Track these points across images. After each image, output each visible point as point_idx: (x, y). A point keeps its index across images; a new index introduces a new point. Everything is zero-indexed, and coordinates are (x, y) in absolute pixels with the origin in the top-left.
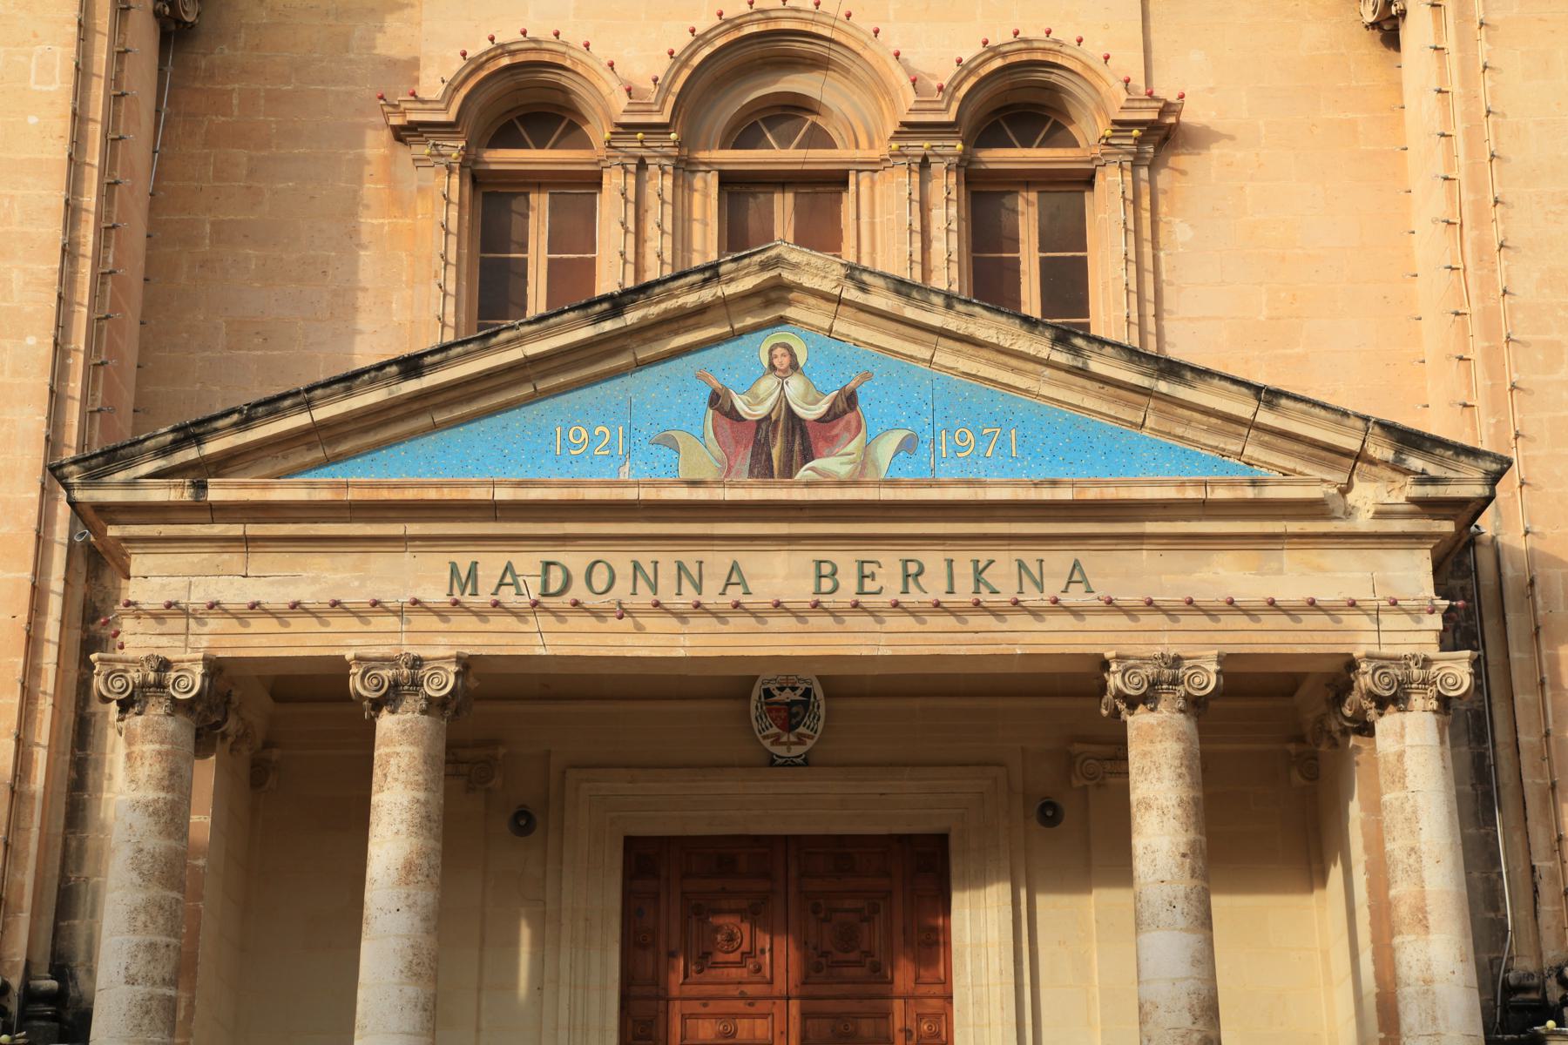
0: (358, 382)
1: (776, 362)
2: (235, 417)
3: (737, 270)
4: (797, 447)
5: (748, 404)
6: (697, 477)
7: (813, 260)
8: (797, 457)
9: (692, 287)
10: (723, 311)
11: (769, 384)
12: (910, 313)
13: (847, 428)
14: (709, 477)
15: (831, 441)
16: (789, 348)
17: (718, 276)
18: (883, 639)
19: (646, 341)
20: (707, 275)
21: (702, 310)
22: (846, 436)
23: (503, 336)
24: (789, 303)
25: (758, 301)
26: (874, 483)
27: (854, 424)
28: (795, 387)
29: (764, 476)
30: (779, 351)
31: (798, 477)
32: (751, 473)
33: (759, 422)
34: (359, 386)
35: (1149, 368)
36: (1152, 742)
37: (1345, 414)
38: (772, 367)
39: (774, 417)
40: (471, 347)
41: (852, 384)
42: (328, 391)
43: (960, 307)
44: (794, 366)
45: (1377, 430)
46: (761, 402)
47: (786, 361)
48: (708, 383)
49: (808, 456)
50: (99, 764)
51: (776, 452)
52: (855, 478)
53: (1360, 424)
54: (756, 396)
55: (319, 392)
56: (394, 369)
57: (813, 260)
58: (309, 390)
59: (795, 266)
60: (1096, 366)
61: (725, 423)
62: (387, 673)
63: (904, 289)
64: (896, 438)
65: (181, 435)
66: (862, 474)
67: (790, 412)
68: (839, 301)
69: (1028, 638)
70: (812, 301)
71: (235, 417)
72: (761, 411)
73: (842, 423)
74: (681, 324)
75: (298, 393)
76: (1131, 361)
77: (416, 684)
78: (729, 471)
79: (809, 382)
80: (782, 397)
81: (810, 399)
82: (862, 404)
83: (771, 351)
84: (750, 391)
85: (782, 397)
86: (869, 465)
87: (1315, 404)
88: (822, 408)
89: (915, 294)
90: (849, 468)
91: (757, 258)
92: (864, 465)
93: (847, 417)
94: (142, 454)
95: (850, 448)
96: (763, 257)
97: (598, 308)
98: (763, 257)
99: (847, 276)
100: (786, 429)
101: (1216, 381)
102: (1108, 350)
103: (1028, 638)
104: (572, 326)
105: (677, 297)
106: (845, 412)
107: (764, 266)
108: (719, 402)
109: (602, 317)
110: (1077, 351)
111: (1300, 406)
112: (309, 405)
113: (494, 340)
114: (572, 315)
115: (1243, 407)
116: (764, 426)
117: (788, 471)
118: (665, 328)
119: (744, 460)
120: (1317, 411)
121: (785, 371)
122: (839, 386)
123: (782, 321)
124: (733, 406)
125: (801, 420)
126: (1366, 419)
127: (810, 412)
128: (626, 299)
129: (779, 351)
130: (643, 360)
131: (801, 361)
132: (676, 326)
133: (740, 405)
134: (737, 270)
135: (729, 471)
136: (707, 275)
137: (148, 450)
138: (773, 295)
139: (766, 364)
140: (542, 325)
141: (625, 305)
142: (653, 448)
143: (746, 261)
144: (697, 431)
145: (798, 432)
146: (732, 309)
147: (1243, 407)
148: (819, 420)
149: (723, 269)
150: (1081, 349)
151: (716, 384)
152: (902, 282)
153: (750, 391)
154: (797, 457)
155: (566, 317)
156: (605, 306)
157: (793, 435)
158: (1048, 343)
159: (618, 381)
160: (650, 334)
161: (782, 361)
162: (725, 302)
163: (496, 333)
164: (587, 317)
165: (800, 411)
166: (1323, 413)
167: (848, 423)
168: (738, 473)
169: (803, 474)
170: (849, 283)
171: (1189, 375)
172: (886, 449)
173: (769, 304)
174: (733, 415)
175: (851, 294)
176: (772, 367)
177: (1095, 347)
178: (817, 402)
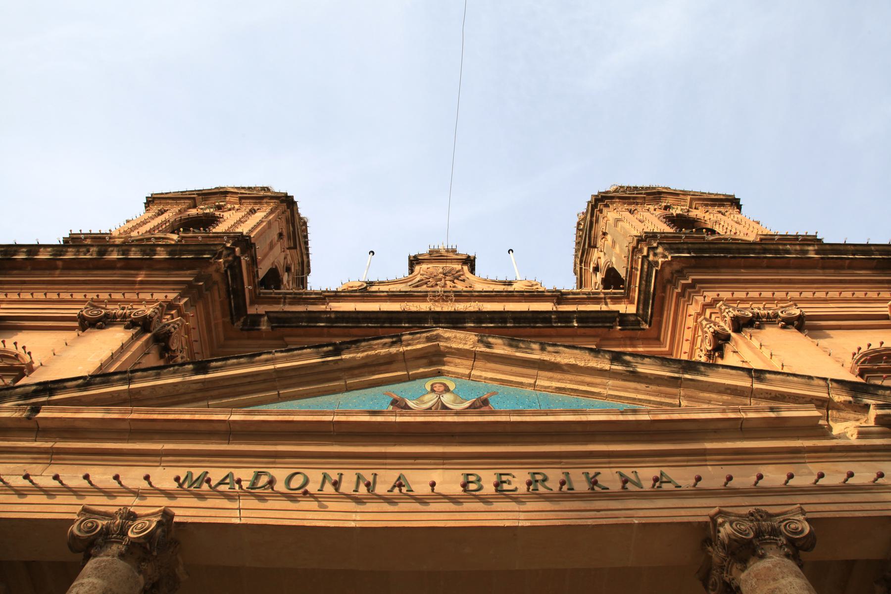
0: (165, 371)
2: (80, 381)
3: (412, 339)
6: (376, 409)
7: (458, 335)
9: (384, 345)
17: (401, 341)
18: (522, 516)
20: (394, 339)
23: (264, 357)
24: (444, 364)
25: (425, 361)
34: (165, 374)
35: (675, 366)
36: (774, 580)
37: (810, 378)
40: (242, 360)
42: (145, 374)
43: (550, 349)
45: (835, 385)
47: (442, 388)
53: (822, 383)
55: (139, 374)
56: (191, 366)
57: (458, 335)
58: (133, 371)
59: (448, 339)
60: (641, 369)
62: (102, 523)
65: (41, 387)
69: (641, 513)
71: (80, 381)
74: (377, 368)
75: (125, 372)
76: (664, 365)
77: (123, 532)
83: (432, 385)
84: (419, 399)
87: (788, 374)
91: (425, 335)
94: (11, 396)
96: (428, 334)
97: (325, 349)
98: (428, 334)
99: (479, 341)
101: (720, 369)
102: (647, 360)
103: (641, 513)
104: (309, 356)
105: (375, 349)
107: (429, 339)
109: (327, 354)
110: (627, 364)
111: (779, 377)
112: (130, 381)
113: (257, 358)
114: (309, 350)
115: (744, 382)
118: (366, 369)
120: (791, 378)
123: (440, 373)
124: (406, 404)
126: (825, 379)
128: (344, 346)
132: (373, 369)
134: (412, 339)
136: (394, 339)
137: (16, 394)
138: (434, 359)
140: (289, 354)
141: (343, 350)
143: (418, 335)
147: (744, 382)
149: (404, 338)
150: (629, 362)
155: (305, 351)
156: (330, 348)
158: (607, 361)
159: (333, 396)
160: (356, 372)
163: (260, 354)
164: (318, 353)
166: (795, 379)
170: (480, 345)
171: (702, 368)
173: (431, 364)
177: (639, 360)
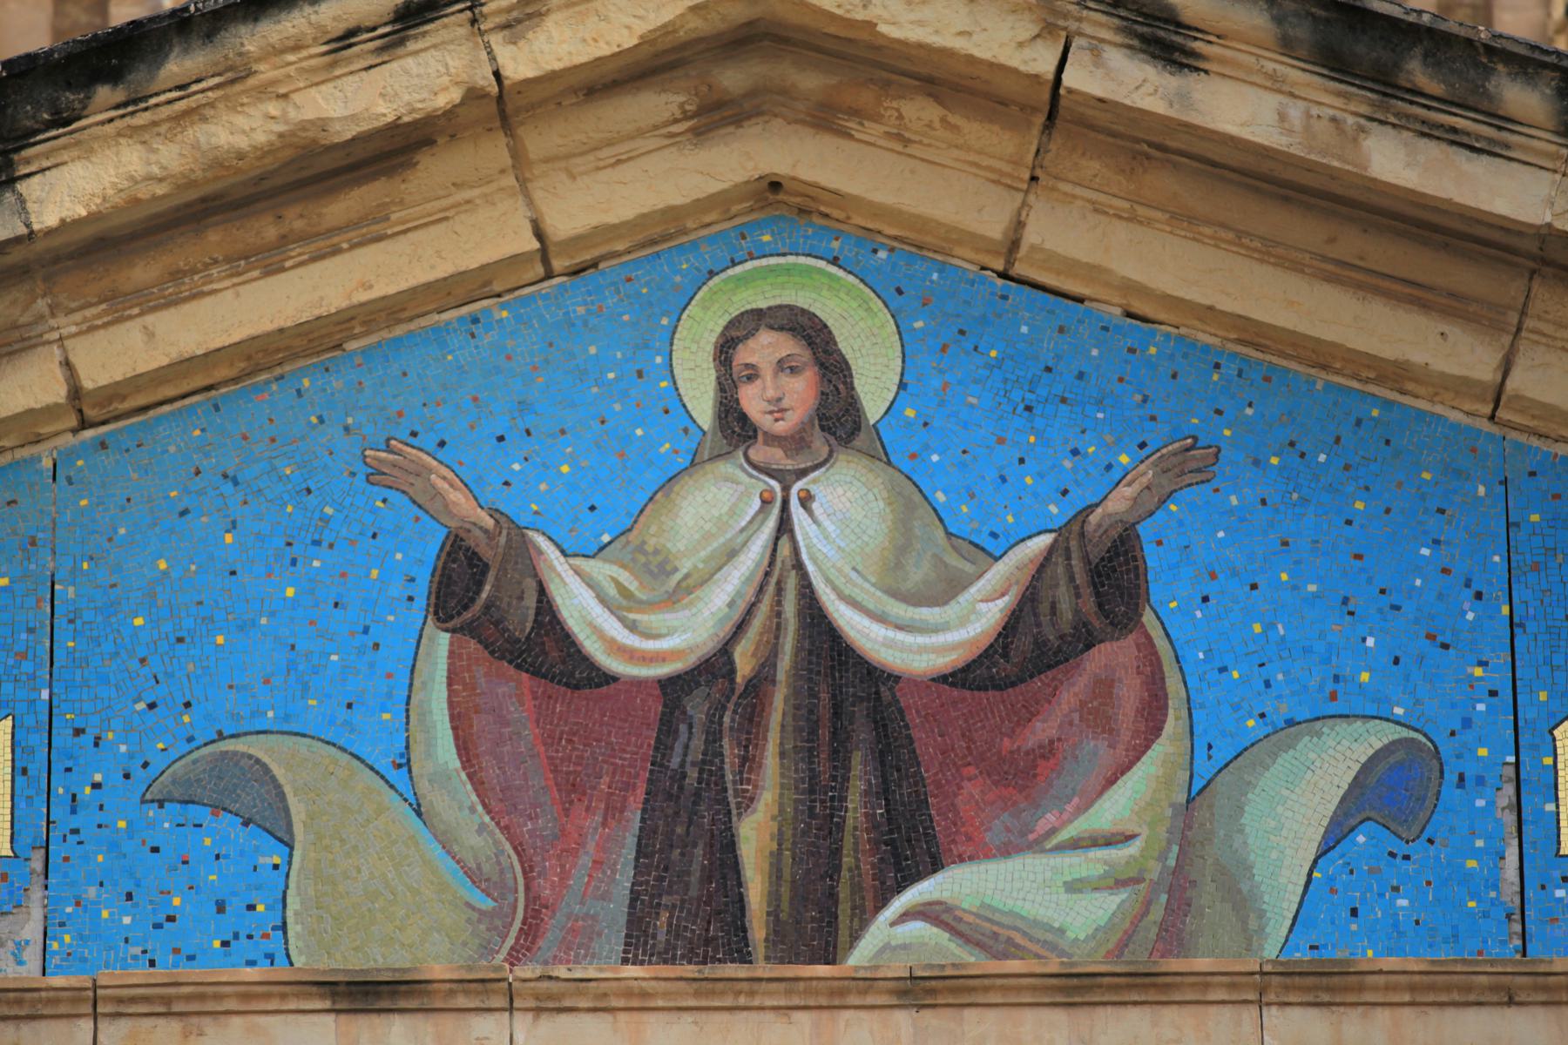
1: (753, 401)
4: (855, 809)
5: (620, 604)
6: (376, 957)
8: (857, 856)
10: (495, 151)
11: (716, 509)
12: (1394, 161)
13: (1097, 715)
14: (438, 962)
15: (1024, 776)
16: (813, 334)
19: (121, 306)
21: (396, 148)
22: (1095, 751)
25: (657, 104)
26: (1234, 980)
27: (1129, 694)
28: (843, 518)
29: (703, 951)
30: (765, 348)
31: (861, 956)
32: (638, 945)
33: (674, 688)
38: (735, 426)
39: (744, 662)
41: (1118, 503)
44: (838, 419)
46: (681, 594)
47: (800, 392)
48: (427, 505)
49: (910, 850)
50: (1183, 219)
51: (755, 836)
52: (1137, 956)
54: (657, 567)
61: (511, 693)
63: (1364, 49)
64: (1332, 761)
66: (1173, 937)
67: (815, 618)
68: (1054, 106)
70: (919, 111)
72: (685, 634)
73: (1073, 690)
74: (295, 219)
78: (531, 931)
79: (911, 496)
80: (784, 569)
81: (918, 573)
82: (1170, 598)
83: (726, 348)
84: (624, 538)
85: (784, 569)
86: (1207, 896)
88: (976, 617)
89: (1417, 72)
90: (1103, 908)
92: (1179, 889)
93: (1098, 659)
95: (1115, 807)
100: (805, 725)
106: (1086, 639)
108: (481, 593)
116: (697, 707)
117: (816, 926)
119: (603, 872)
121: (795, 442)
122: (1057, 512)
125: (875, 677)
127: (916, 641)
129: (765, 348)
130: (114, 392)
131: (874, 391)
133: (581, 605)
135: (531, 931)
138: (733, 78)
139: (704, 410)
142: (164, 821)
144: (377, 734)
145: (863, 734)
146: (539, 140)
148: (963, 678)
151: (453, 524)
152: (625, 588)
153: (624, 538)
154: (857, 856)
157: (840, 756)
160: (142, 272)
161: (781, 395)
162: (501, 108)
165: (866, 634)
167: (1104, 687)
168: (579, 942)
169: (891, 936)
172: (1287, 814)
174: (544, 652)
175: (1116, 76)
176: (735, 426)
178: (947, 589)
